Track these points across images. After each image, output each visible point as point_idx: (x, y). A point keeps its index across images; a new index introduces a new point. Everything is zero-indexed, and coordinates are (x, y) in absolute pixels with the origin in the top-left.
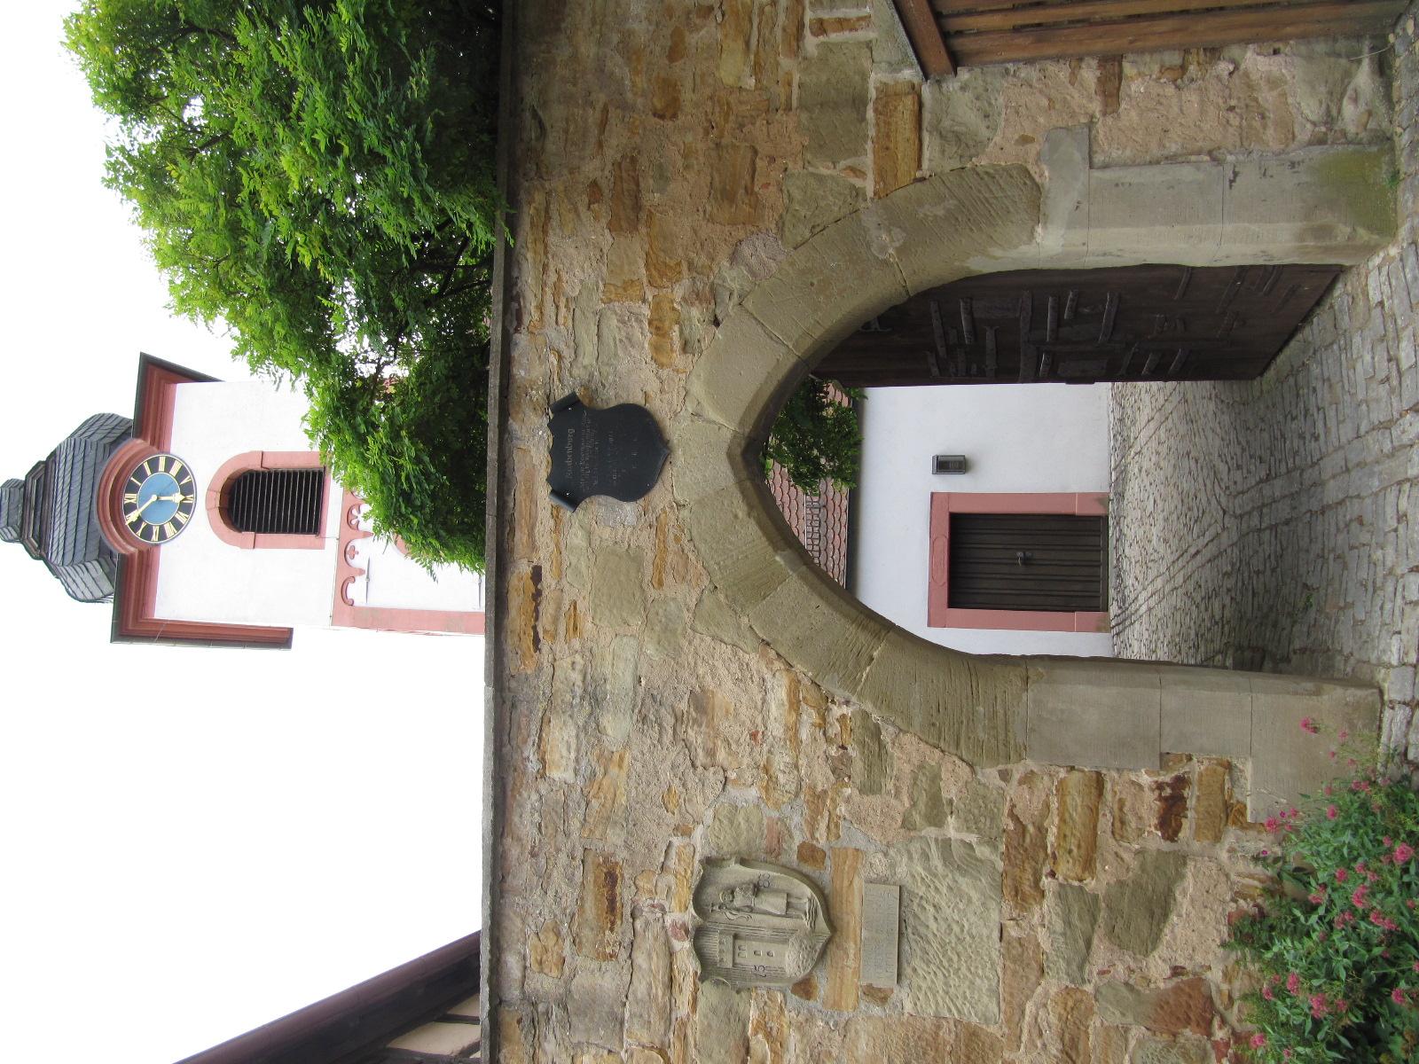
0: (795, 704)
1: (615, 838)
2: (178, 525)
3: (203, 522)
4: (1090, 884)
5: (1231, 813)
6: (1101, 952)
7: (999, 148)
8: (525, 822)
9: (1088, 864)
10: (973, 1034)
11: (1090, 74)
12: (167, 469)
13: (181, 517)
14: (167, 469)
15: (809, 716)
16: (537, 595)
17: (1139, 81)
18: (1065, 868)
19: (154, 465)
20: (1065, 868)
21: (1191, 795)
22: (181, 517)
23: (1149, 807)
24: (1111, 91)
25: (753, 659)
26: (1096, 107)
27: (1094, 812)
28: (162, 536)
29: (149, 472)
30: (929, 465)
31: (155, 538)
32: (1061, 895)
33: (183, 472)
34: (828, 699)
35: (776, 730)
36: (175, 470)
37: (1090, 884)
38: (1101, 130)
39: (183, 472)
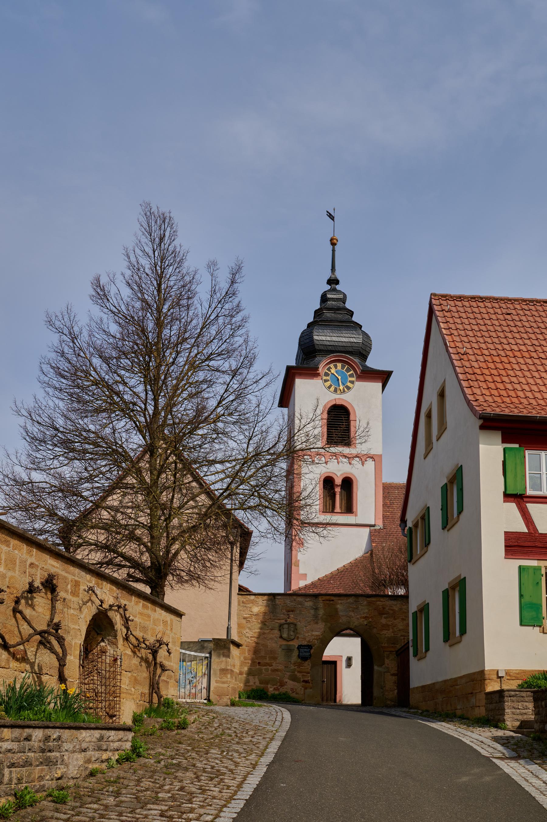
0: (317, 636)
1: (298, 612)
2: (329, 387)
3: (330, 398)
4: (296, 672)
5: (306, 688)
6: (288, 674)
7: (387, 661)
8: (300, 599)
9: (299, 672)
10: (277, 658)
11: (396, 672)
12: (350, 382)
13: (332, 389)
14: (350, 382)
15: (316, 637)
16: (330, 601)
17: (394, 678)
18: (298, 669)
19: (351, 376)
20: (298, 669)
21: (308, 684)
22: (332, 389)
23: (306, 679)
24: (393, 675)
25: (323, 630)
26: (392, 673)
27: (305, 672)
28: (326, 381)
29: (349, 374)
30: (350, 655)
31: (324, 378)
32: (295, 669)
33: (349, 388)
34: (317, 640)
35: (314, 633)
36: (349, 384)
37: (296, 672)
38: (389, 674)
39: (349, 388)
